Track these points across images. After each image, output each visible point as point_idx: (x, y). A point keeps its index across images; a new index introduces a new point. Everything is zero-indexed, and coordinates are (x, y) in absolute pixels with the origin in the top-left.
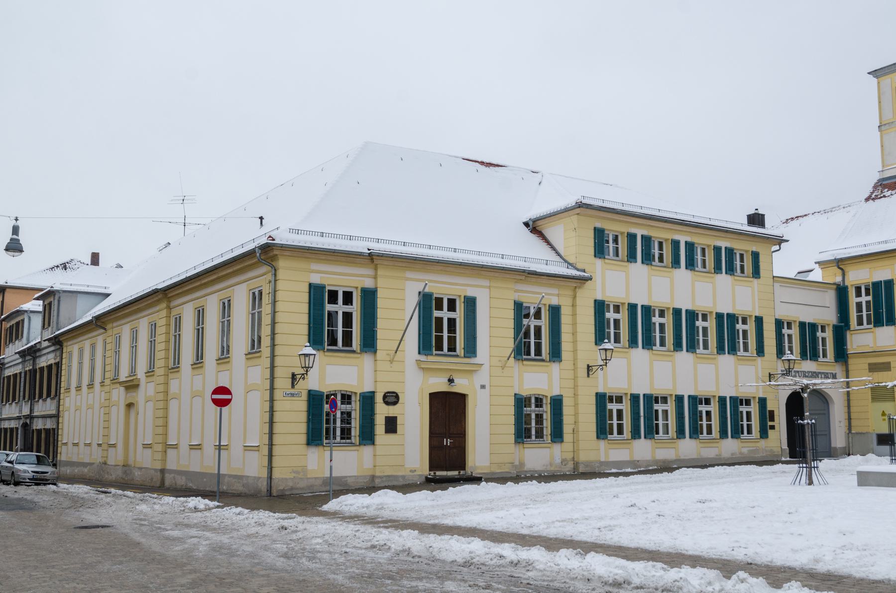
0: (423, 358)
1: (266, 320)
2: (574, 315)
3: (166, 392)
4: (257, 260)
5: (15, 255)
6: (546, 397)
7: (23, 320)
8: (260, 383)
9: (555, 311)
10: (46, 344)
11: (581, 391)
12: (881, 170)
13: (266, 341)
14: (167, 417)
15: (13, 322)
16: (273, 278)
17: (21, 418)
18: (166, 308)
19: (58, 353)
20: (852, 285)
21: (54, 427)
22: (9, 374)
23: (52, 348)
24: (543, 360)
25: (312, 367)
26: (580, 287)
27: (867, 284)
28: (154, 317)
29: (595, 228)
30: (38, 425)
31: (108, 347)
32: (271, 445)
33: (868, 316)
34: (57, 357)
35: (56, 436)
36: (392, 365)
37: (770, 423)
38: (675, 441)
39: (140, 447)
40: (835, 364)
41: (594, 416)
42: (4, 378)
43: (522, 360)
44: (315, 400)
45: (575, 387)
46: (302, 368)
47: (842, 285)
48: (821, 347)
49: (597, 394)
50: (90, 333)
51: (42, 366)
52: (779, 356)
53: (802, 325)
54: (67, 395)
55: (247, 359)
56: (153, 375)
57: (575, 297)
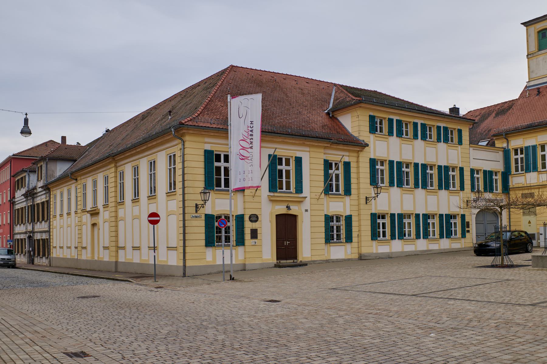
0: (272, 194)
1: (179, 172)
2: (358, 167)
3: (116, 217)
4: (173, 136)
5: (27, 136)
6: (342, 216)
7: (25, 176)
8: (176, 210)
9: (347, 165)
10: (40, 190)
11: (362, 212)
12: (528, 81)
13: (179, 185)
14: (117, 231)
15: (19, 177)
16: (183, 146)
17: (27, 233)
18: (114, 167)
19: (48, 195)
20: (512, 149)
21: (47, 238)
22: (18, 208)
23: (44, 192)
24: (340, 195)
25: (208, 200)
26: (361, 151)
27: (522, 148)
28: (107, 173)
29: (370, 115)
30: (38, 236)
31: (79, 191)
32: (184, 246)
33: (522, 166)
34: (47, 197)
35: (49, 243)
36: (253, 198)
37: (467, 229)
38: (460, 239)
39: (101, 249)
40: (502, 194)
41: (370, 227)
42: (15, 210)
43: (329, 195)
44: (209, 219)
45: (359, 210)
46: (202, 200)
47: (507, 148)
48: (494, 185)
49: (371, 214)
50: (62, 184)
51: (38, 202)
52: (473, 190)
53: (485, 172)
54: (54, 219)
55: (167, 196)
56: (108, 207)
57: (358, 157)
